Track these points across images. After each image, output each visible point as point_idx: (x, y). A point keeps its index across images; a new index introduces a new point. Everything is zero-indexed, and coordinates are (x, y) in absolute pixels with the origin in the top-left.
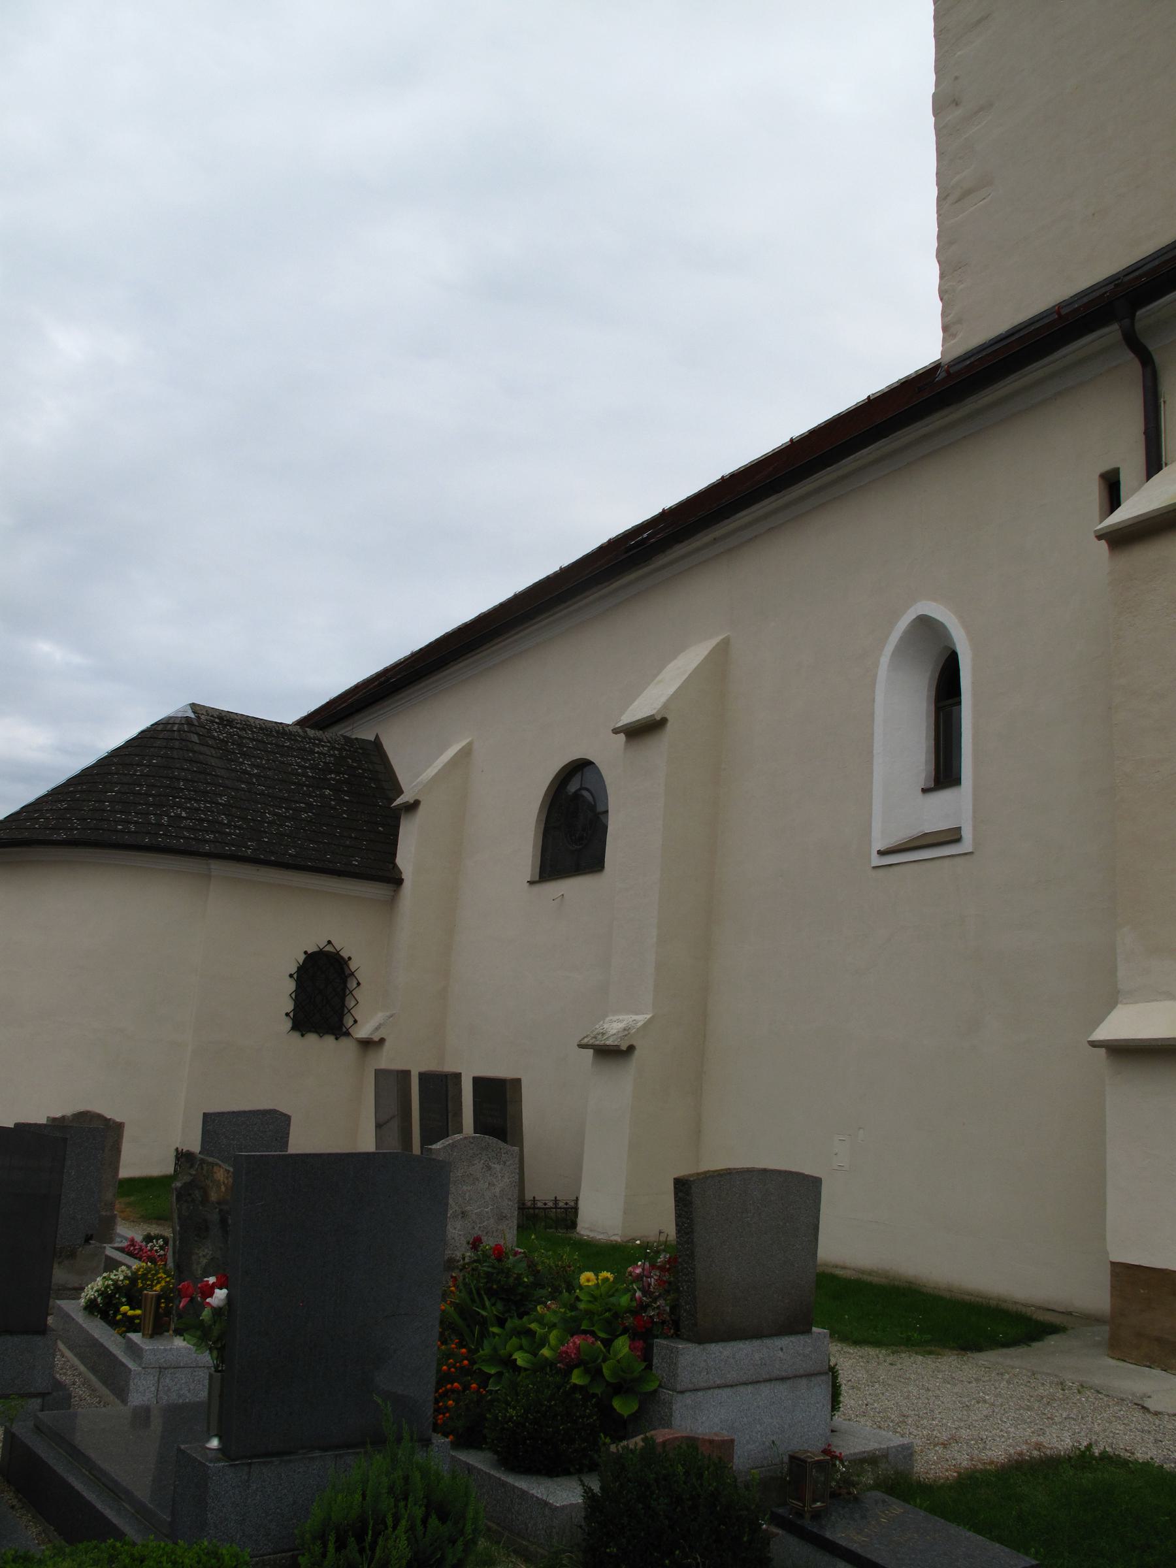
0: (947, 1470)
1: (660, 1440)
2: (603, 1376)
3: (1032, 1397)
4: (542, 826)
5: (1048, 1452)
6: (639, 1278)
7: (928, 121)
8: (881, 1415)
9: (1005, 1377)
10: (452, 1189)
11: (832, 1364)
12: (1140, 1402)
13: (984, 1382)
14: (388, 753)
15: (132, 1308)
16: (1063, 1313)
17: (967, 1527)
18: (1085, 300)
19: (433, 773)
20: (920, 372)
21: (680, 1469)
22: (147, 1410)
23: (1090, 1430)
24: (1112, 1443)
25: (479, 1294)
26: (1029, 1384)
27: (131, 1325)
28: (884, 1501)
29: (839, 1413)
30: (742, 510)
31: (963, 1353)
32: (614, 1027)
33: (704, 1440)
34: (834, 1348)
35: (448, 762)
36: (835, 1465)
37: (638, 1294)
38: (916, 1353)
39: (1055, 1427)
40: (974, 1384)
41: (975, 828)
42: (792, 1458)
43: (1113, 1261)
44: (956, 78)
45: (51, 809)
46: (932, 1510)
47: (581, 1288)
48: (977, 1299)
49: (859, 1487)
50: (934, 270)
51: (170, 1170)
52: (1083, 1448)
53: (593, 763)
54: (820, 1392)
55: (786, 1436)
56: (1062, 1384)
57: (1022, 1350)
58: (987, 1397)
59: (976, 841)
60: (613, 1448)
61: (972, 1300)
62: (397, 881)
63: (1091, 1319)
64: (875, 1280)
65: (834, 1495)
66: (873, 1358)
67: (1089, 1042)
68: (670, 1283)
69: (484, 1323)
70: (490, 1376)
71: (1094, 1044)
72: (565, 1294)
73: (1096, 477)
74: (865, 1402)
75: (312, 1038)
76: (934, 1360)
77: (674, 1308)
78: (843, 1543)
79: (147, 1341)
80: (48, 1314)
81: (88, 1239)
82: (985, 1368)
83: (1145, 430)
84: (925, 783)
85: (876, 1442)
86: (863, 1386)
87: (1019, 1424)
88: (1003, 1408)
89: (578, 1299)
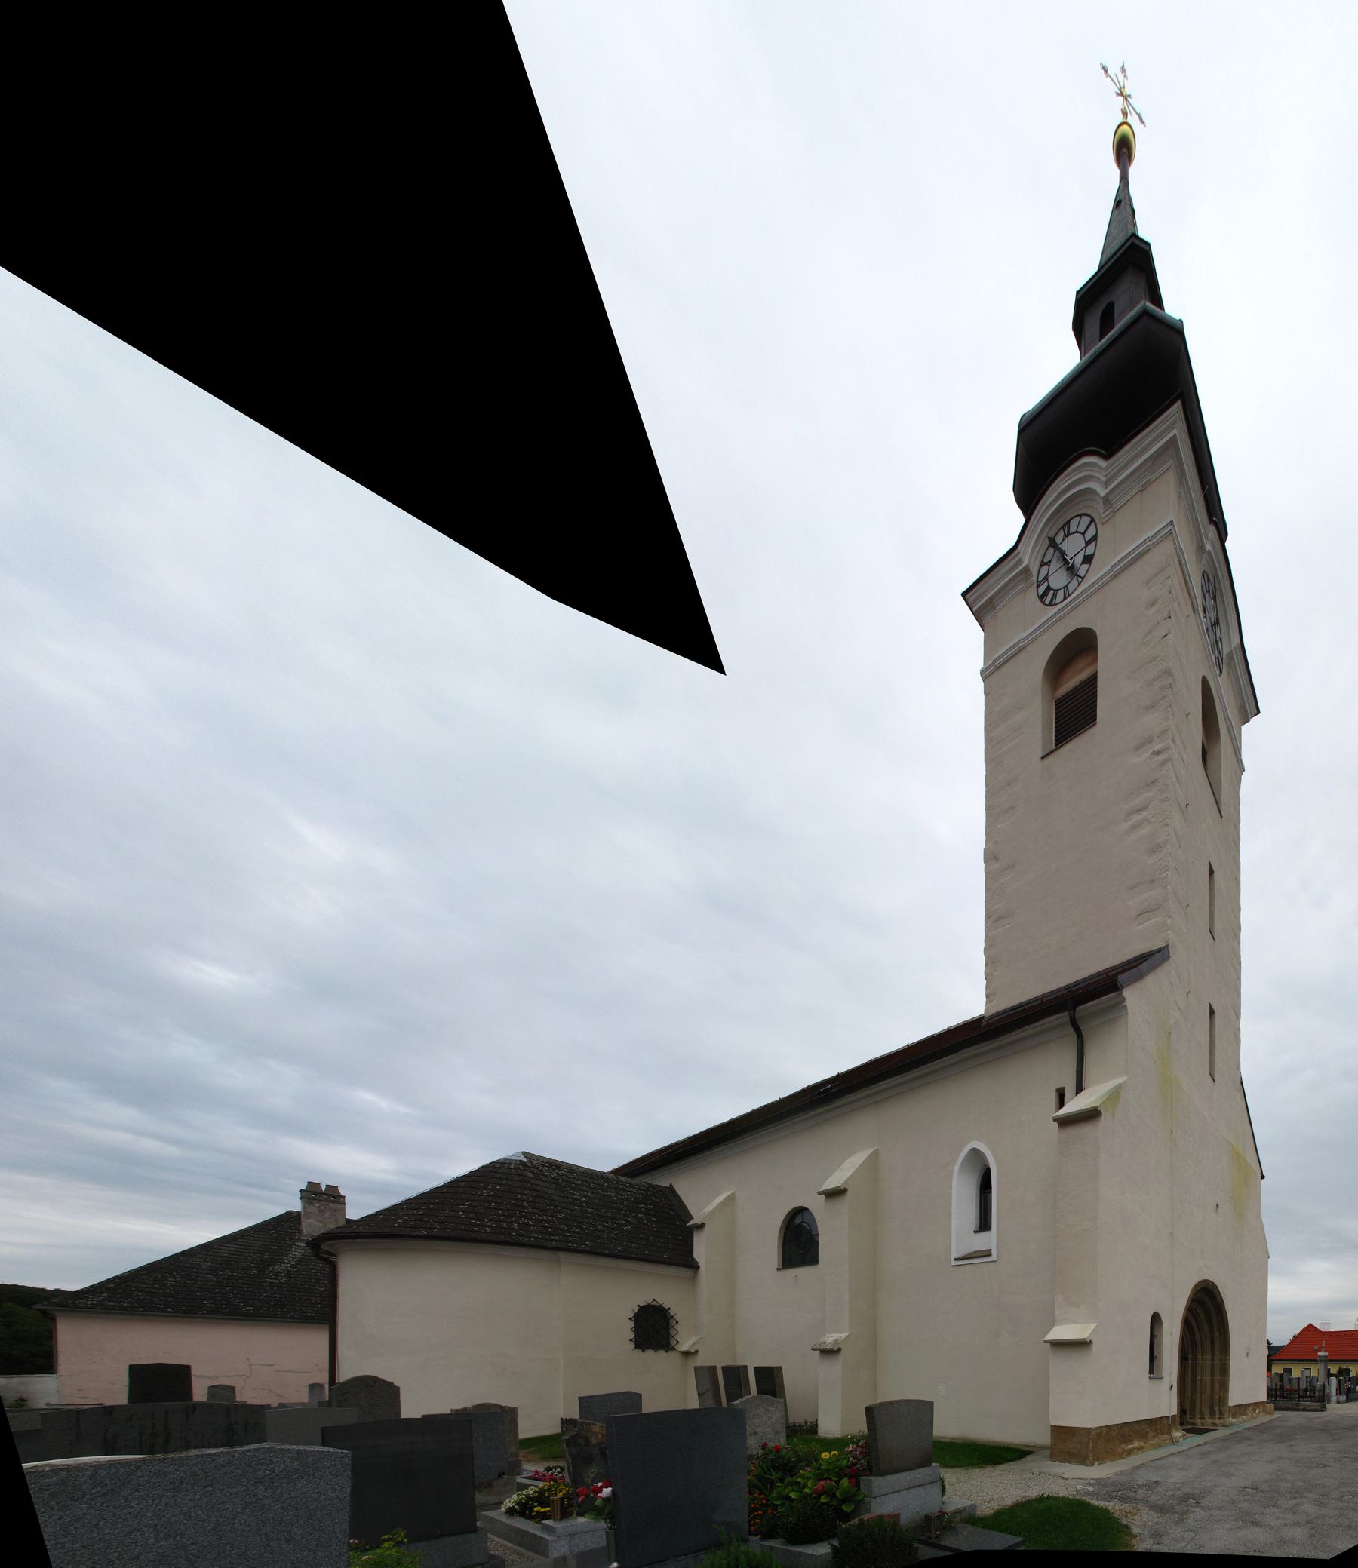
1: (866, 1519)
2: (836, 1497)
4: (782, 1240)
6: (851, 1452)
7: (981, 866)
10: (748, 1422)
14: (688, 1207)
15: (542, 1508)
18: (1054, 996)
19: (712, 1209)
21: (876, 1529)
22: (564, 1559)
25: (768, 1469)
27: (544, 1516)
32: (829, 1340)
33: (886, 1516)
34: (942, 1470)
35: (721, 1203)
37: (851, 1459)
41: (997, 1250)
42: (926, 1516)
44: (996, 842)
45: (408, 1214)
46: (984, 1527)
47: (822, 1460)
51: (559, 1430)
53: (807, 1209)
54: (937, 1488)
57: (1018, 1462)
59: (998, 1257)
60: (844, 1526)
62: (695, 1267)
63: (1043, 1448)
64: (958, 1441)
65: (944, 1528)
68: (866, 1453)
69: (772, 1482)
70: (777, 1505)
71: (1045, 1342)
72: (814, 1464)
73: (1054, 1090)
75: (650, 1353)
77: (869, 1463)
78: (950, 1545)
79: (557, 1523)
80: (476, 1521)
81: (501, 1475)
89: (821, 1465)
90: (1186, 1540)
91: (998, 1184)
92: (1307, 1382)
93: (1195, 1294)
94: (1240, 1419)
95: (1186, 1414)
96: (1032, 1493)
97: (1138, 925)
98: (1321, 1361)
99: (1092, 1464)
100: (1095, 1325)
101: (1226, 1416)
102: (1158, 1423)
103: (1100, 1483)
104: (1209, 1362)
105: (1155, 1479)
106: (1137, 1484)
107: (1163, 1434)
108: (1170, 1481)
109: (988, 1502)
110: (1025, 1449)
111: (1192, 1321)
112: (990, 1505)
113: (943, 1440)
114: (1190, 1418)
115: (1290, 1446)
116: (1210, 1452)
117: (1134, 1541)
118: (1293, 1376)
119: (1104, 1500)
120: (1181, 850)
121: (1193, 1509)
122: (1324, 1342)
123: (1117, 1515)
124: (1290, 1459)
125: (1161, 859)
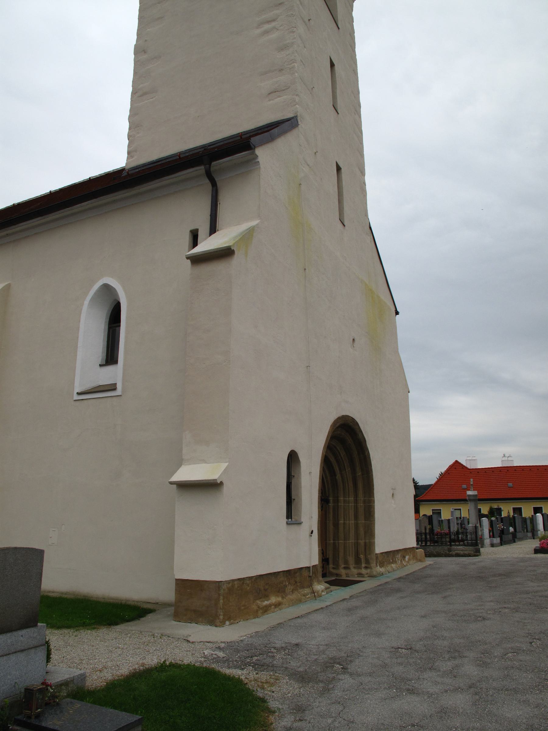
0: (101, 682)
3: (140, 643)
5: (147, 667)
8: (71, 661)
9: (128, 635)
11: (47, 640)
12: (186, 639)
13: (119, 639)
16: (154, 603)
17: (111, 707)
18: (191, 153)
20: (116, 170)
23: (165, 654)
24: (175, 658)
26: (139, 637)
28: (71, 703)
29: (50, 663)
30: (24, 222)
31: (110, 627)
34: (48, 632)
36: (48, 689)
38: (88, 629)
39: (150, 655)
40: (114, 641)
41: (123, 384)
43: (177, 578)
44: (146, 41)
46: (94, 703)
48: (116, 601)
49: (59, 698)
50: (127, 125)
52: (162, 662)
54: (41, 654)
55: (23, 679)
56: (153, 635)
58: (120, 646)
61: (114, 602)
63: (166, 605)
64: (68, 596)
65: (47, 704)
66: (67, 634)
67: (169, 482)
71: (171, 483)
73: (189, 231)
74: (63, 656)
76: (96, 632)
82: (120, 632)
83: (211, 214)
84: (101, 362)
85: (68, 675)
86: (62, 648)
87: (134, 656)
88: (127, 650)
90: (334, 715)
91: (128, 318)
92: (457, 524)
93: (334, 431)
94: (389, 568)
95: (328, 564)
96: (152, 660)
97: (270, 100)
98: (470, 500)
99: (222, 624)
100: (227, 464)
101: (373, 565)
102: (298, 574)
103: (230, 646)
104: (352, 505)
105: (294, 641)
106: (275, 648)
107: (303, 587)
108: (313, 642)
109: (100, 671)
110: (145, 606)
111: (332, 460)
112: (102, 675)
113: (51, 594)
114: (333, 568)
115: (445, 597)
116: (356, 607)
117: (272, 718)
118: (443, 518)
119: (236, 667)
120: (305, 49)
121: (340, 677)
122: (472, 480)
123: (251, 686)
124: (445, 612)
125: (289, 54)
